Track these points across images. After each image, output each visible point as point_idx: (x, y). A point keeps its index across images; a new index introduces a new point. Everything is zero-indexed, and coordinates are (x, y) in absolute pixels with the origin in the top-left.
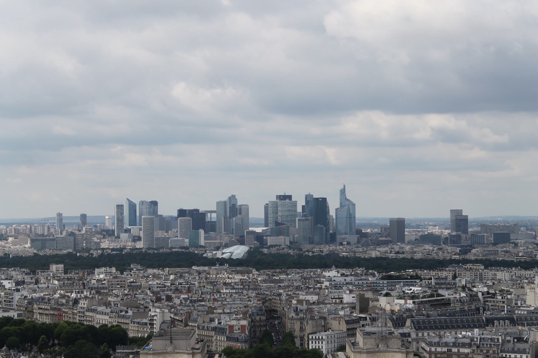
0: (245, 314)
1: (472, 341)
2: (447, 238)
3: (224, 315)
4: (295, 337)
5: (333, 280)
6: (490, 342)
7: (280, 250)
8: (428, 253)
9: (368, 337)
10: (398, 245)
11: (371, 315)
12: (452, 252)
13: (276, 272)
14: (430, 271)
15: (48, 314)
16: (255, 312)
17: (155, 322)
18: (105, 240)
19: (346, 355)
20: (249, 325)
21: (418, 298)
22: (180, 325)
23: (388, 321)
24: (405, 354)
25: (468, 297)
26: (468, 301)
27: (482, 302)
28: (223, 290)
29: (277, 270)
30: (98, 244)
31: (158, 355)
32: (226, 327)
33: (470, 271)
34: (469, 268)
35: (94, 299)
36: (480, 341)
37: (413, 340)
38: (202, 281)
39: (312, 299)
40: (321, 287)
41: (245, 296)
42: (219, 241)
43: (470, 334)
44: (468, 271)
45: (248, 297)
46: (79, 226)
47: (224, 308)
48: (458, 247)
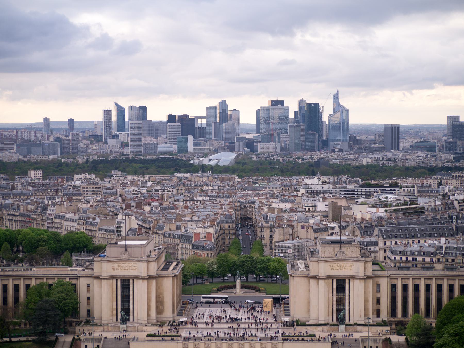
0: (213, 221)
1: (437, 250)
2: (443, 146)
3: (191, 222)
5: (309, 188)
6: (455, 251)
7: (269, 157)
8: (420, 161)
9: (327, 245)
10: (392, 152)
11: (340, 223)
12: (445, 159)
14: (415, 178)
15: (17, 220)
16: (224, 220)
17: (121, 229)
18: (92, 146)
19: (307, 263)
20: (216, 233)
21: (391, 206)
22: (148, 233)
23: (356, 230)
24: (364, 263)
25: (443, 205)
26: (443, 209)
27: (458, 210)
28: (197, 197)
29: (260, 178)
31: (113, 263)
32: (191, 235)
33: (456, 179)
34: (458, 176)
35: (62, 205)
36: (446, 250)
37: (380, 248)
38: (180, 188)
39: (285, 207)
40: (297, 194)
41: (217, 203)
42: (208, 148)
43: (436, 242)
44: (454, 179)
45: (221, 205)
46: (66, 131)
47: (193, 216)
48: (452, 154)
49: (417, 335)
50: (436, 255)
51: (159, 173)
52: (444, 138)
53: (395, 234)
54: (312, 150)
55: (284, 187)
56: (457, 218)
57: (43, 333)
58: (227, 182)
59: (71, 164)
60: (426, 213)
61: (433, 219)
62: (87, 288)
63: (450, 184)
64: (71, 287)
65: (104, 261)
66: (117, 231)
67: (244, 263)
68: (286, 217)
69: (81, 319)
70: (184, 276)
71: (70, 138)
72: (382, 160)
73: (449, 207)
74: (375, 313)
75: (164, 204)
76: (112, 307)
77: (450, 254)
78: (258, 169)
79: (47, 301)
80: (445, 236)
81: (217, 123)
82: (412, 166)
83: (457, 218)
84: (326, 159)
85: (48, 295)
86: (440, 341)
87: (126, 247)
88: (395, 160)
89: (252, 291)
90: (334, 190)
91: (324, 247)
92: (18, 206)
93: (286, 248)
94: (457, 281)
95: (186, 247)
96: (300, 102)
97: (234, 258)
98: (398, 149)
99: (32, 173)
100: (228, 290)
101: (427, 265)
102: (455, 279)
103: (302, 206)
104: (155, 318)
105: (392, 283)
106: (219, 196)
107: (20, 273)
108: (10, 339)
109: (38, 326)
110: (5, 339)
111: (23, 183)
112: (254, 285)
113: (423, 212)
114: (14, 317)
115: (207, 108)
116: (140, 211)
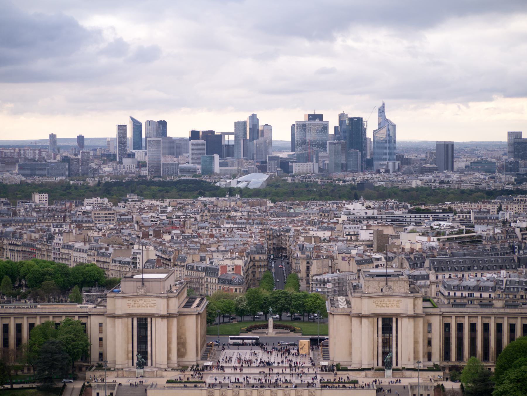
0: (241, 252)
1: (496, 285)
2: (503, 166)
3: (217, 253)
4: (300, 279)
5: (351, 214)
6: (517, 286)
7: (306, 178)
8: (477, 183)
9: (371, 279)
10: (445, 173)
11: (387, 254)
12: (506, 181)
13: (293, 204)
14: (471, 203)
15: (19, 251)
16: (254, 251)
17: (138, 261)
18: (105, 166)
19: (348, 300)
20: (245, 265)
21: (444, 235)
22: (168, 265)
23: (404, 262)
24: (413, 299)
25: (503, 233)
26: (503, 238)
27: (520, 239)
28: (223, 225)
29: (296, 202)
30: (97, 170)
31: (128, 299)
32: (217, 267)
33: (518, 204)
34: (520, 200)
35: (71, 234)
36: (506, 285)
37: (432, 283)
38: (204, 214)
39: (324, 235)
40: (337, 221)
41: (247, 232)
42: (237, 168)
43: (496, 276)
44: (516, 203)
45: (251, 233)
46: (75, 149)
47: (219, 246)
48: (513, 175)
49: (474, 381)
50: (495, 290)
51: (180, 197)
52: (505, 157)
53: (449, 266)
54: (354, 171)
55: (323, 212)
56: (520, 248)
57: (49, 379)
58: (258, 208)
59: (81, 186)
60: (484, 242)
61: (492, 249)
62: (99, 328)
63: (511, 209)
64: (80, 327)
65: (118, 298)
66: (133, 263)
67: (277, 299)
68: (325, 247)
69: (92, 363)
70: (209, 314)
71: (80, 157)
72: (434, 182)
73: (510, 236)
74: (426, 356)
75: (186, 232)
76: (127, 350)
77: (512, 290)
78: (293, 193)
79: (53, 343)
80: (506, 268)
81: (246, 140)
82: (468, 189)
83: (520, 248)
84: (370, 181)
85: (55, 335)
86: (500, 389)
87: (143, 281)
88: (448, 182)
89: (286, 331)
90: (379, 216)
91: (369, 281)
92: (21, 234)
93: (325, 282)
94: (519, 320)
95: (212, 281)
96: (341, 116)
97: (265, 293)
98: (452, 169)
99: (37, 197)
100: (259, 331)
101: (485, 302)
102: (517, 317)
103: (343, 234)
104: (176, 362)
105: (446, 322)
106: (249, 223)
107: (23, 311)
108: (12, 386)
109: (43, 370)
110: (6, 386)
111: (26, 209)
112: (289, 324)
113: (480, 242)
114: (16, 360)
115: (235, 123)
116: (159, 240)
